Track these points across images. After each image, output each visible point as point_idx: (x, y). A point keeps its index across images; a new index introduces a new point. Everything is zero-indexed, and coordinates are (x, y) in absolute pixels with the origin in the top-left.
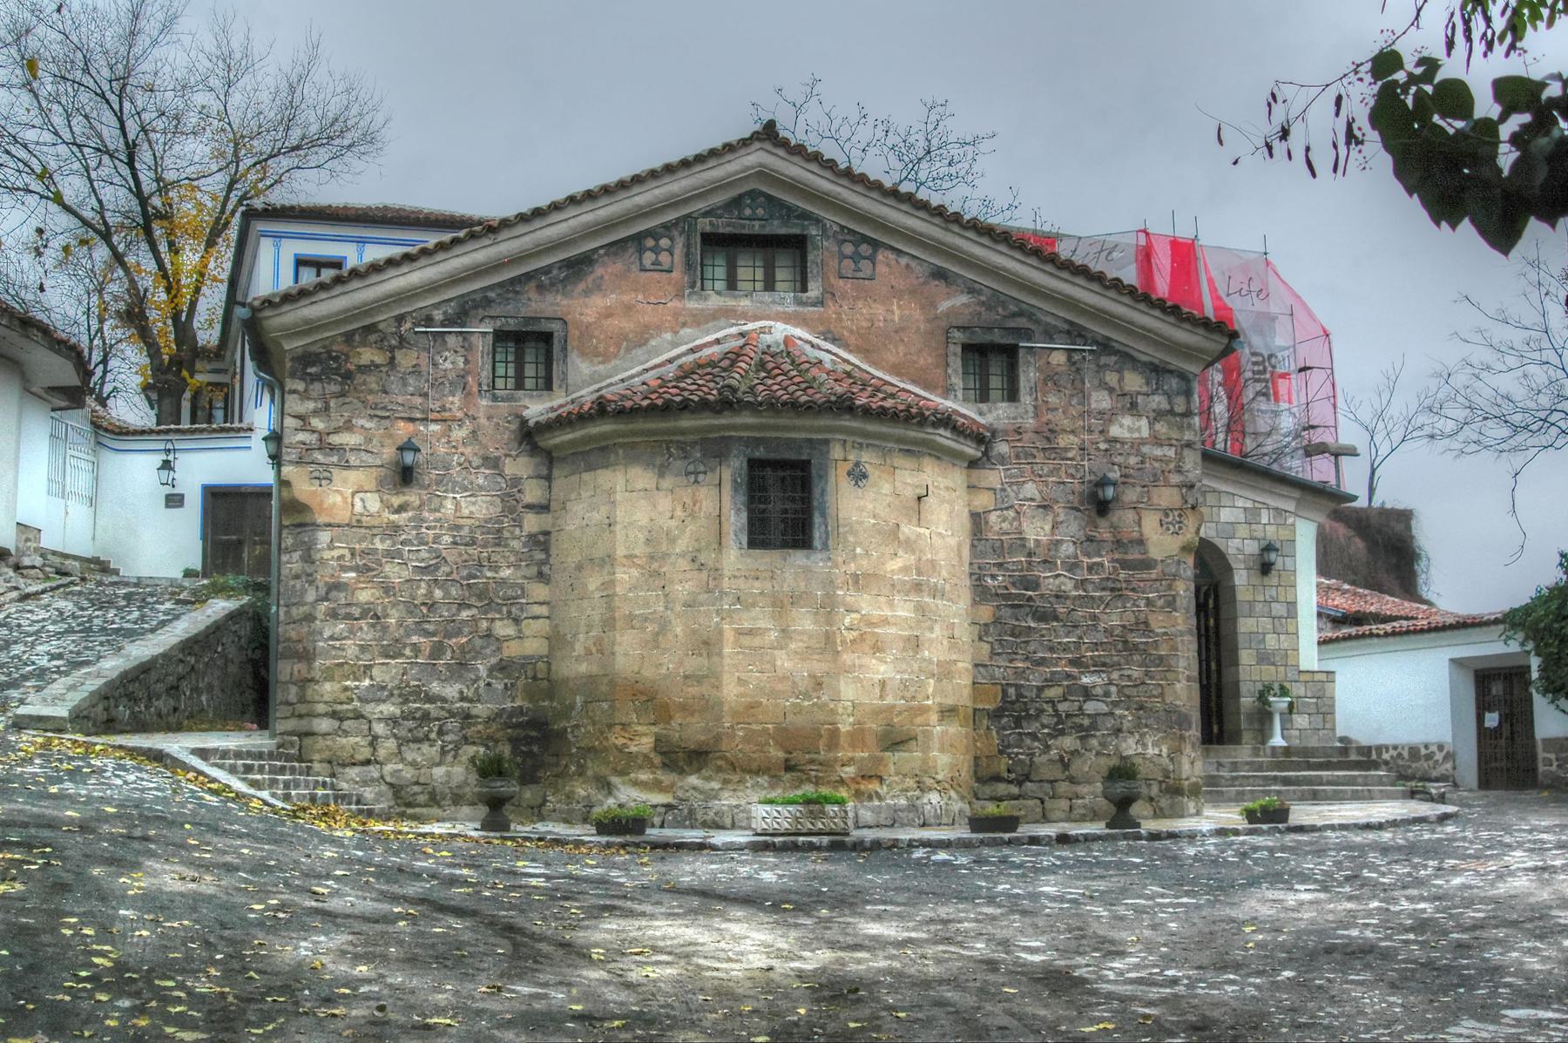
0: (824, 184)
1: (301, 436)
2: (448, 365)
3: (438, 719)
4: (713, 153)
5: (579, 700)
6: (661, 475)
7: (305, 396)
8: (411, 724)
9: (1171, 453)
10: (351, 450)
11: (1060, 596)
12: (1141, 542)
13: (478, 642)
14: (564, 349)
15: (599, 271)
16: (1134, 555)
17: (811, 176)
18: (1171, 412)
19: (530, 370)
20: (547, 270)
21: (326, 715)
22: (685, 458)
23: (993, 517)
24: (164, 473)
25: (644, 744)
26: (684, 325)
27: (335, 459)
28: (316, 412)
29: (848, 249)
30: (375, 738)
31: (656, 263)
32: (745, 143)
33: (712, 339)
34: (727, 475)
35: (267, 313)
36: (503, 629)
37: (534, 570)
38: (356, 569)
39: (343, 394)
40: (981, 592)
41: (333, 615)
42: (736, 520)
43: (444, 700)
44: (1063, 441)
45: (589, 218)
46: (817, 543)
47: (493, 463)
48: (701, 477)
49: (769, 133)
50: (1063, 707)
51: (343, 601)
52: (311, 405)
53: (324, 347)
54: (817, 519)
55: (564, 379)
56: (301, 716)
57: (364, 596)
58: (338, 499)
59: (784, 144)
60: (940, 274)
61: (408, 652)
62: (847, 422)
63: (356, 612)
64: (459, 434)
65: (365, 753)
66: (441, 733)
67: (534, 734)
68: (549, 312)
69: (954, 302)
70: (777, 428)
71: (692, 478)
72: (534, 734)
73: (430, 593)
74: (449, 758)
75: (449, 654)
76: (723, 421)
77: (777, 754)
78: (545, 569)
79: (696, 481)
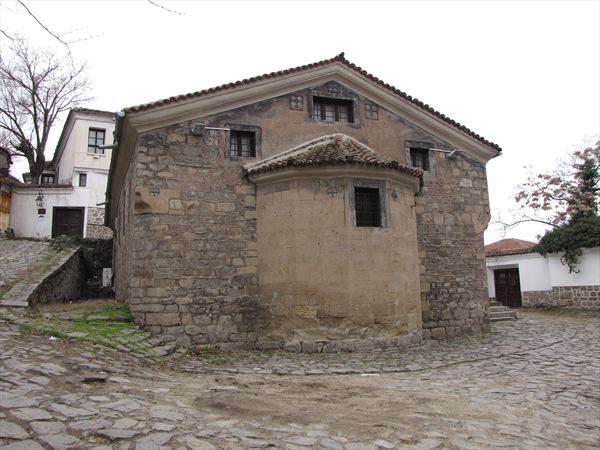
0: (361, 81)
1: (145, 173)
2: (211, 144)
5: (275, 294)
7: (147, 154)
8: (197, 306)
9: (479, 192)
11: (448, 247)
12: (472, 226)
13: (227, 268)
14: (260, 140)
15: (273, 108)
16: (470, 231)
18: (479, 178)
19: (244, 148)
20: (253, 106)
21: (158, 303)
23: (424, 216)
24: (38, 202)
25: (312, 313)
27: (161, 183)
28: (152, 162)
29: (368, 107)
30: (181, 313)
31: (296, 106)
32: (332, 60)
33: (323, 140)
34: (347, 195)
35: (132, 114)
36: (237, 262)
37: (250, 236)
38: (171, 235)
39: (165, 154)
40: (422, 246)
41: (160, 256)
42: (352, 214)
43: (211, 295)
44: (446, 187)
45: (272, 85)
46: (383, 225)
47: (231, 188)
49: (341, 58)
50: (451, 290)
52: (150, 159)
54: (382, 214)
55: (261, 153)
56: (145, 303)
57: (175, 247)
58: (162, 202)
59: (347, 63)
60: (401, 120)
61: (195, 272)
62: (394, 173)
63: (171, 254)
64: (216, 174)
65: (177, 320)
66: (211, 310)
67: (252, 309)
68: (253, 124)
69: (406, 132)
70: (367, 174)
72: (252, 309)
73: (205, 245)
74: (215, 321)
75: (213, 273)
76: (347, 170)
77: (372, 316)
78: (255, 235)
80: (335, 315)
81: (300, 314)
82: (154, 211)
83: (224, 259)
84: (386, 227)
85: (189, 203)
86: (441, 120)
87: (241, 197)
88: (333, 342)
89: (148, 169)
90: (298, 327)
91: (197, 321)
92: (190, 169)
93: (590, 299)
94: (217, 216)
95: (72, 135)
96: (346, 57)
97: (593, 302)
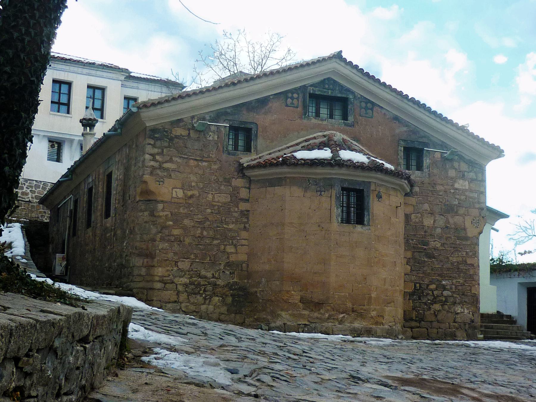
2: (211, 138)
3: (204, 285)
6: (306, 191)
22: (316, 185)
26: (302, 129)
43: (206, 277)
48: (323, 193)
51: (167, 234)
63: (173, 239)
65: (174, 298)
71: (319, 193)
72: (241, 293)
79: (321, 195)
82: (159, 199)
83: (218, 245)
85: (189, 193)
87: (236, 189)
89: (154, 160)
90: (282, 310)
92: (192, 161)
94: (214, 206)
96: (344, 55)
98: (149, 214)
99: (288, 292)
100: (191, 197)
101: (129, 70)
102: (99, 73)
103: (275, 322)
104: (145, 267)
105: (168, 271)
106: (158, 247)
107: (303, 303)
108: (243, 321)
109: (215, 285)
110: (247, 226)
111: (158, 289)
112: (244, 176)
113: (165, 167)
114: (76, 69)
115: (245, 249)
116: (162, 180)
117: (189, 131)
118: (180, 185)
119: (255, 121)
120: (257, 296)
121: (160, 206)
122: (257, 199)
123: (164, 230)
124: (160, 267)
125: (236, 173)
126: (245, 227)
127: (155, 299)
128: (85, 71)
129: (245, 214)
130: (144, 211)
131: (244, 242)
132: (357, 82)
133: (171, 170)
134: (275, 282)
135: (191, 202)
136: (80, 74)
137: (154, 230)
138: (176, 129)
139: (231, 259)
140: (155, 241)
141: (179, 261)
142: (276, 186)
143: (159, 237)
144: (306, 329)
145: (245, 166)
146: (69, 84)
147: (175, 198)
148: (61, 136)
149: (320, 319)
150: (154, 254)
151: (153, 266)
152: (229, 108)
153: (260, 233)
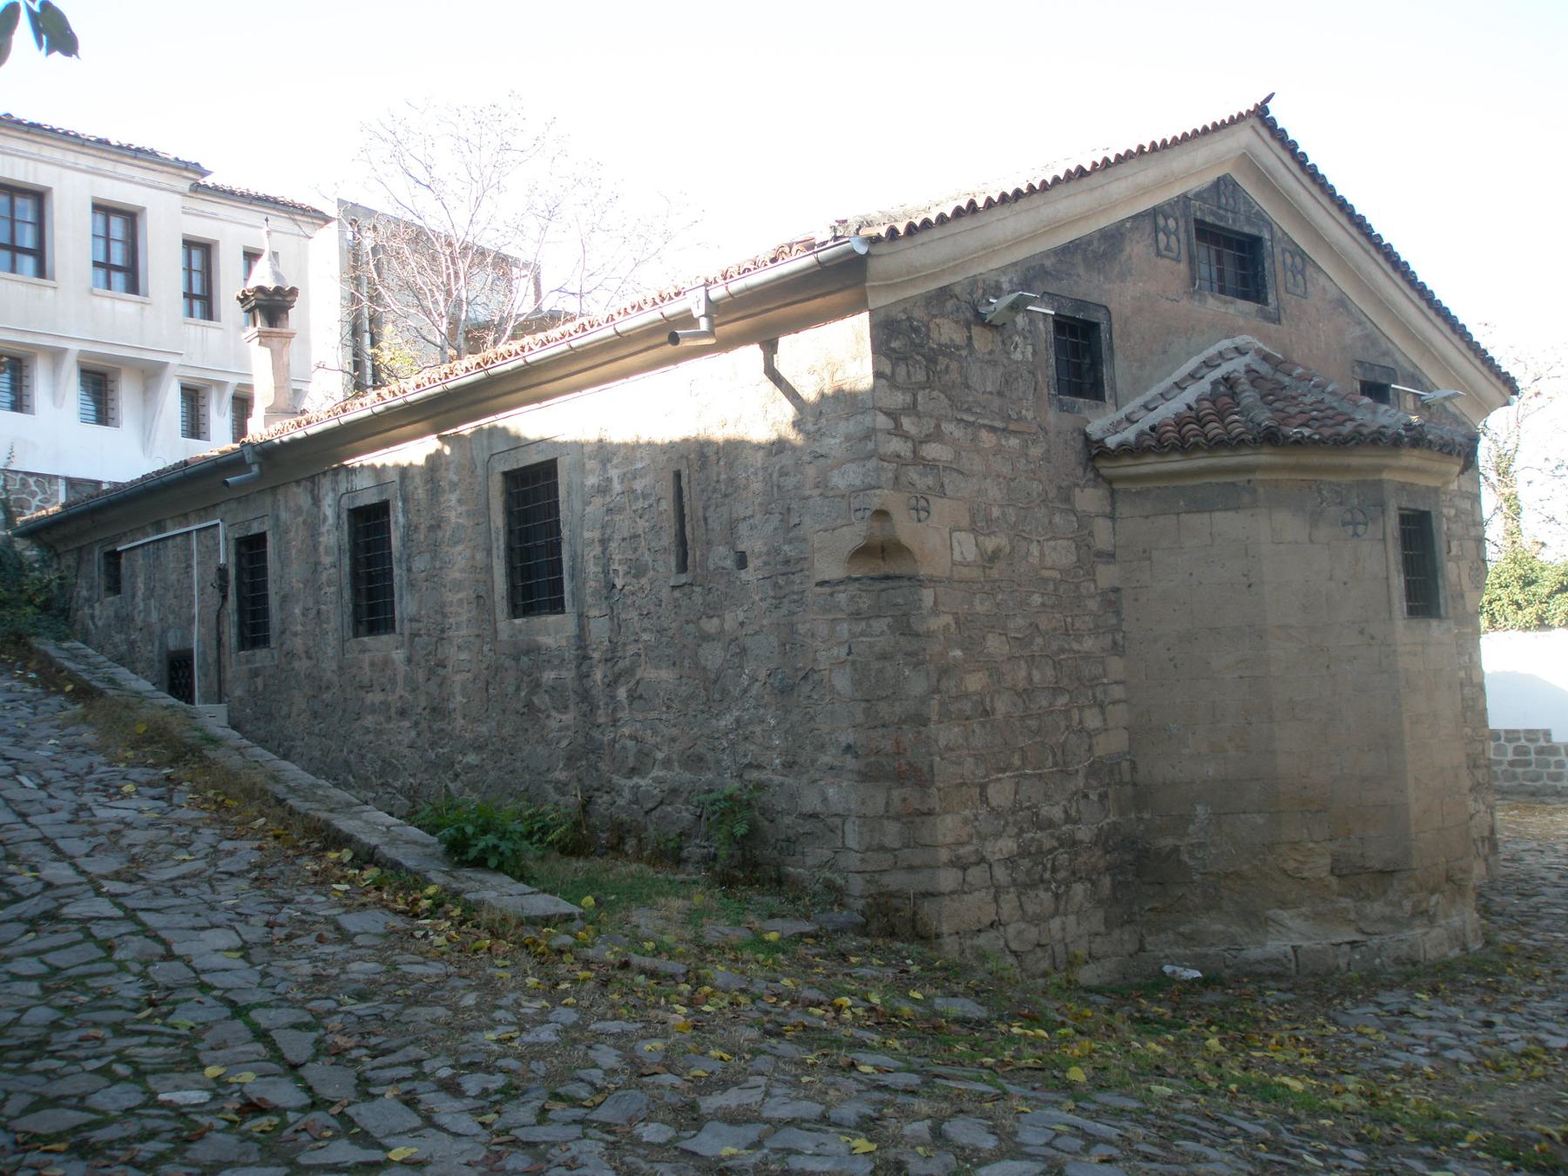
2: (1018, 356)
4: (1217, 128)
10: (945, 468)
17: (1283, 170)
22: (1341, 504)
25: (1320, 866)
27: (930, 481)
43: (1051, 824)
48: (1361, 529)
49: (1261, 113)
51: (953, 692)
53: (905, 311)
56: (911, 868)
63: (967, 706)
65: (988, 916)
71: (1350, 529)
72: (1128, 857)
79: (1355, 534)
80: (1378, 866)
81: (1290, 865)
82: (924, 571)
83: (1066, 713)
84: (1447, 618)
85: (990, 544)
86: (1423, 305)
87: (1084, 520)
88: (1375, 941)
89: (898, 432)
90: (1283, 905)
91: (1031, 908)
92: (984, 434)
93: (1512, 763)
94: (1045, 580)
95: (150, 274)
96: (1274, 110)
97: (1520, 770)
98: (888, 625)
99: (1294, 845)
100: (994, 556)
101: (202, 165)
102: (122, 169)
103: (1262, 944)
104: (897, 818)
105: (966, 821)
106: (937, 742)
107: (1339, 876)
108: (1137, 946)
109: (1072, 844)
110: (1119, 637)
111: (953, 893)
112: (1100, 479)
113: (929, 458)
114: (57, 154)
115: (1119, 714)
116: (922, 503)
117: (969, 330)
118: (965, 522)
119: (1104, 301)
120: (1179, 861)
121: (928, 596)
122: (1145, 551)
123: (944, 684)
124: (948, 812)
125: (1079, 472)
126: (1115, 643)
127: (945, 929)
128: (85, 161)
129: (1112, 599)
130: (869, 618)
131: (1118, 692)
132: (1287, 192)
133: (941, 465)
134: (1249, 816)
135: (995, 574)
136: (69, 168)
137: (917, 685)
138: (937, 321)
139: (1099, 751)
140: (925, 722)
141: (990, 781)
142: (1219, 510)
143: (936, 708)
144: (1357, 957)
145: (1112, 447)
146: (39, 196)
147: (961, 564)
148: (28, 339)
149: (1391, 920)
150: (926, 769)
151: (930, 813)
152: (1046, 254)
153: (1171, 660)
